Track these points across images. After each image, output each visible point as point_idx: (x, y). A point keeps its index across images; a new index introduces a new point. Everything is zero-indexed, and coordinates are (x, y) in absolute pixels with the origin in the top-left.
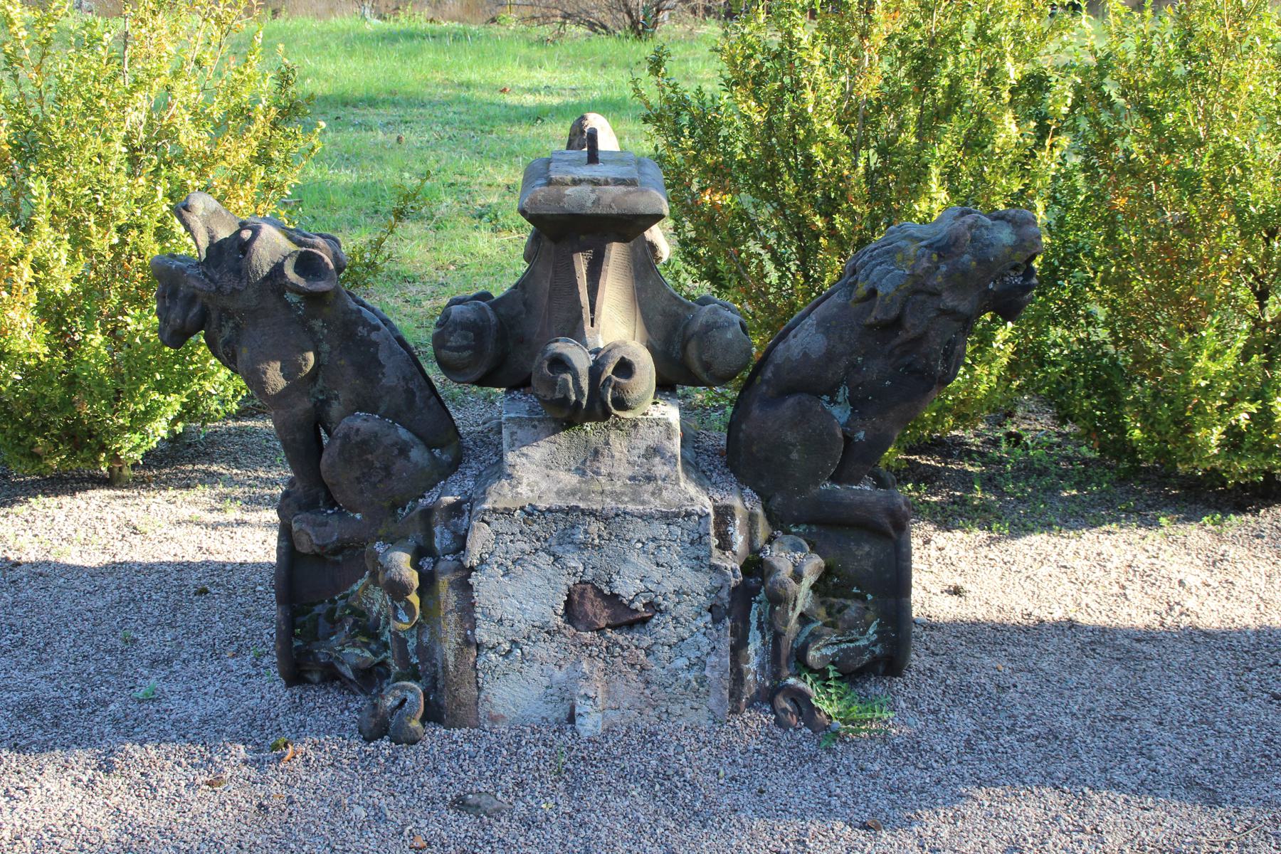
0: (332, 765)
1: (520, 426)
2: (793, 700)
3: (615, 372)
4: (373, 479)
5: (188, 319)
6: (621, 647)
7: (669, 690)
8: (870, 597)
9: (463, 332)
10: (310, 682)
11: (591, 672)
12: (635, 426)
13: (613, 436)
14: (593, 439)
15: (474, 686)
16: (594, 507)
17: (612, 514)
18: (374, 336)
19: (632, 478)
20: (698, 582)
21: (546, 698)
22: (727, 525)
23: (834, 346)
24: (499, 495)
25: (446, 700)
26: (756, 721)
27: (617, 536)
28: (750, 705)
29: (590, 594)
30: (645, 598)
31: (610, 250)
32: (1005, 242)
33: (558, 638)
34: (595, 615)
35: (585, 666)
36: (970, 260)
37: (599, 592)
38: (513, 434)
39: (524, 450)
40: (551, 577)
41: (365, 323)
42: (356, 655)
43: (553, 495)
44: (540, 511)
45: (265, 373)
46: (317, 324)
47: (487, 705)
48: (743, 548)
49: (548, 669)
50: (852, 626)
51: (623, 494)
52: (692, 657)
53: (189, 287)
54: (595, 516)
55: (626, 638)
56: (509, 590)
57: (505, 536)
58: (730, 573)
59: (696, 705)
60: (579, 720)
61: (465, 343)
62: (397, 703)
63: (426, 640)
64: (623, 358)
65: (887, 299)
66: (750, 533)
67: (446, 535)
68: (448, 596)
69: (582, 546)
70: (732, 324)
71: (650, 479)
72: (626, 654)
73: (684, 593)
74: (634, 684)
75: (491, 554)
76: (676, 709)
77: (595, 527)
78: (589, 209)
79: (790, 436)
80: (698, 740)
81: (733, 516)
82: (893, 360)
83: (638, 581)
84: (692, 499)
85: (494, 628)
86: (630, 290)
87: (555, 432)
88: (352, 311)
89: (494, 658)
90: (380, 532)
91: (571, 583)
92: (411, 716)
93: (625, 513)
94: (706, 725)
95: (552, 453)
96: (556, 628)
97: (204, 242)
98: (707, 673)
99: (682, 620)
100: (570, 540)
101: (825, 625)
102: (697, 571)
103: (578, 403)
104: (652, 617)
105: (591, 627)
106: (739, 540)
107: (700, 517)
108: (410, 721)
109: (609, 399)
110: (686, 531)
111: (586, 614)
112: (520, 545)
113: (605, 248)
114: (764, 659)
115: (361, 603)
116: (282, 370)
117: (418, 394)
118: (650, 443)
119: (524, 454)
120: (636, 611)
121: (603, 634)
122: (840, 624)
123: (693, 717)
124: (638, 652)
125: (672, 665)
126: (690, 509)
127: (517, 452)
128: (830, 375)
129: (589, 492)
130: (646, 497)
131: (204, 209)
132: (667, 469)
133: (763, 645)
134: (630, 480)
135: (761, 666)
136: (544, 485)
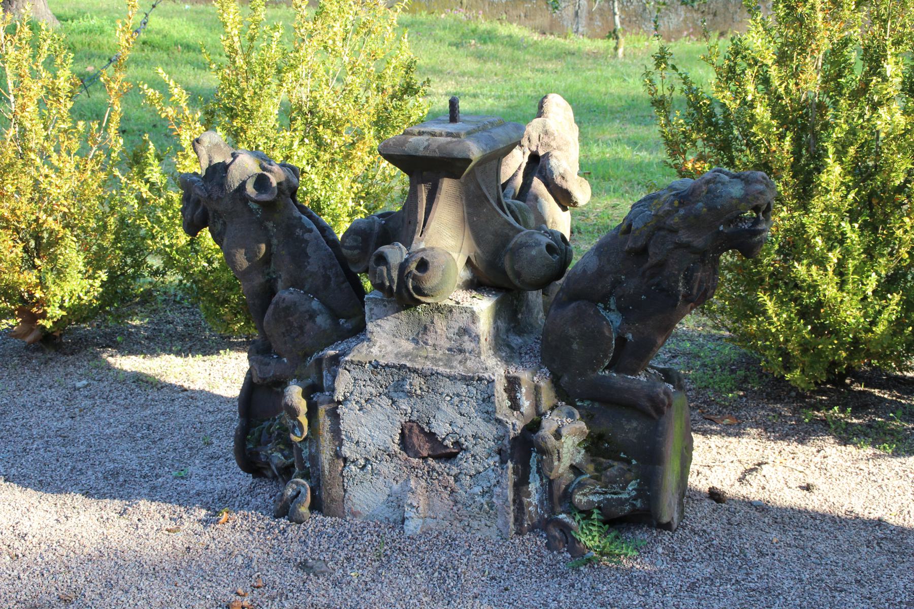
0: (248, 530)
1: (376, 305)
2: (561, 530)
3: (417, 268)
4: (293, 335)
5: (195, 215)
6: (437, 472)
7: (469, 509)
8: (634, 462)
9: (355, 237)
10: (266, 477)
11: (416, 488)
12: (451, 311)
13: (436, 317)
14: (423, 318)
15: (341, 487)
16: (417, 367)
17: (429, 373)
18: (306, 236)
19: (450, 350)
20: (489, 431)
21: (388, 503)
22: (516, 392)
23: (603, 266)
24: (360, 352)
25: (324, 495)
26: (536, 542)
27: (433, 390)
28: (532, 529)
29: (416, 430)
30: (452, 438)
31: (442, 183)
32: (733, 195)
33: (395, 459)
34: (420, 446)
35: (412, 483)
36: (702, 207)
37: (422, 430)
38: (371, 309)
39: (379, 322)
40: (390, 414)
41: (303, 226)
42: (278, 458)
43: (393, 356)
44: (381, 366)
45: (235, 256)
46: (270, 225)
47: (350, 503)
48: (530, 411)
49: (389, 482)
50: (613, 481)
51: (440, 360)
52: (485, 486)
53: (195, 194)
54: (417, 373)
55: (441, 467)
56: (363, 421)
57: (360, 382)
58: (511, 427)
59: (489, 523)
60: (406, 522)
61: (355, 244)
62: (295, 493)
63: (313, 451)
64: (422, 259)
65: (637, 232)
66: (536, 400)
67: (329, 378)
68: (325, 422)
69: (409, 395)
70: (538, 244)
71: (461, 351)
72: (441, 478)
73: (479, 438)
74: (446, 501)
75: (351, 393)
76: (475, 524)
77: (417, 381)
78: (421, 152)
79: (571, 331)
80: (484, 549)
81: (520, 385)
82: (646, 279)
83: (448, 425)
84: (486, 369)
85: (353, 447)
86: (461, 214)
87: (398, 311)
88: (295, 218)
89: (354, 470)
90: (296, 372)
91: (403, 421)
92: (301, 503)
93: (438, 373)
94: (495, 538)
95: (397, 326)
96: (393, 453)
97: (205, 164)
98: (494, 500)
99: (477, 457)
100: (402, 389)
101: (591, 477)
102: (487, 422)
103: (391, 287)
104: (458, 453)
105: (417, 455)
106: (526, 404)
107: (489, 382)
108: (300, 507)
109: (411, 287)
110: (479, 392)
111: (414, 445)
112: (369, 389)
113: (438, 182)
114: (542, 496)
115: (286, 422)
116: (245, 254)
117: (333, 279)
118: (461, 325)
119: (378, 325)
120: (447, 447)
121: (426, 462)
122: (603, 478)
123: (486, 532)
124: (449, 478)
125: (472, 490)
126: (481, 375)
127: (374, 323)
128: (600, 288)
129: (417, 357)
130: (455, 363)
131: (210, 142)
132: (473, 345)
133: (542, 485)
134: (448, 351)
135: (541, 501)
136: (389, 348)
